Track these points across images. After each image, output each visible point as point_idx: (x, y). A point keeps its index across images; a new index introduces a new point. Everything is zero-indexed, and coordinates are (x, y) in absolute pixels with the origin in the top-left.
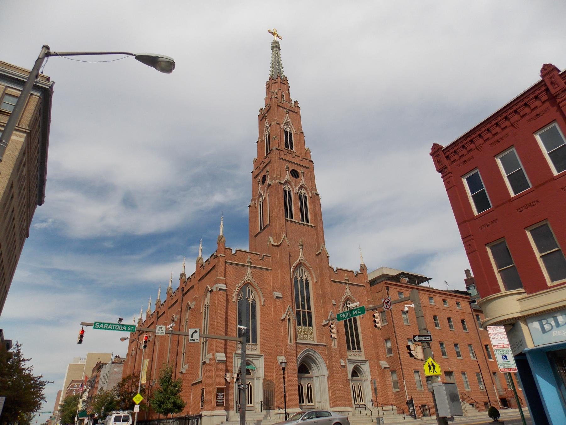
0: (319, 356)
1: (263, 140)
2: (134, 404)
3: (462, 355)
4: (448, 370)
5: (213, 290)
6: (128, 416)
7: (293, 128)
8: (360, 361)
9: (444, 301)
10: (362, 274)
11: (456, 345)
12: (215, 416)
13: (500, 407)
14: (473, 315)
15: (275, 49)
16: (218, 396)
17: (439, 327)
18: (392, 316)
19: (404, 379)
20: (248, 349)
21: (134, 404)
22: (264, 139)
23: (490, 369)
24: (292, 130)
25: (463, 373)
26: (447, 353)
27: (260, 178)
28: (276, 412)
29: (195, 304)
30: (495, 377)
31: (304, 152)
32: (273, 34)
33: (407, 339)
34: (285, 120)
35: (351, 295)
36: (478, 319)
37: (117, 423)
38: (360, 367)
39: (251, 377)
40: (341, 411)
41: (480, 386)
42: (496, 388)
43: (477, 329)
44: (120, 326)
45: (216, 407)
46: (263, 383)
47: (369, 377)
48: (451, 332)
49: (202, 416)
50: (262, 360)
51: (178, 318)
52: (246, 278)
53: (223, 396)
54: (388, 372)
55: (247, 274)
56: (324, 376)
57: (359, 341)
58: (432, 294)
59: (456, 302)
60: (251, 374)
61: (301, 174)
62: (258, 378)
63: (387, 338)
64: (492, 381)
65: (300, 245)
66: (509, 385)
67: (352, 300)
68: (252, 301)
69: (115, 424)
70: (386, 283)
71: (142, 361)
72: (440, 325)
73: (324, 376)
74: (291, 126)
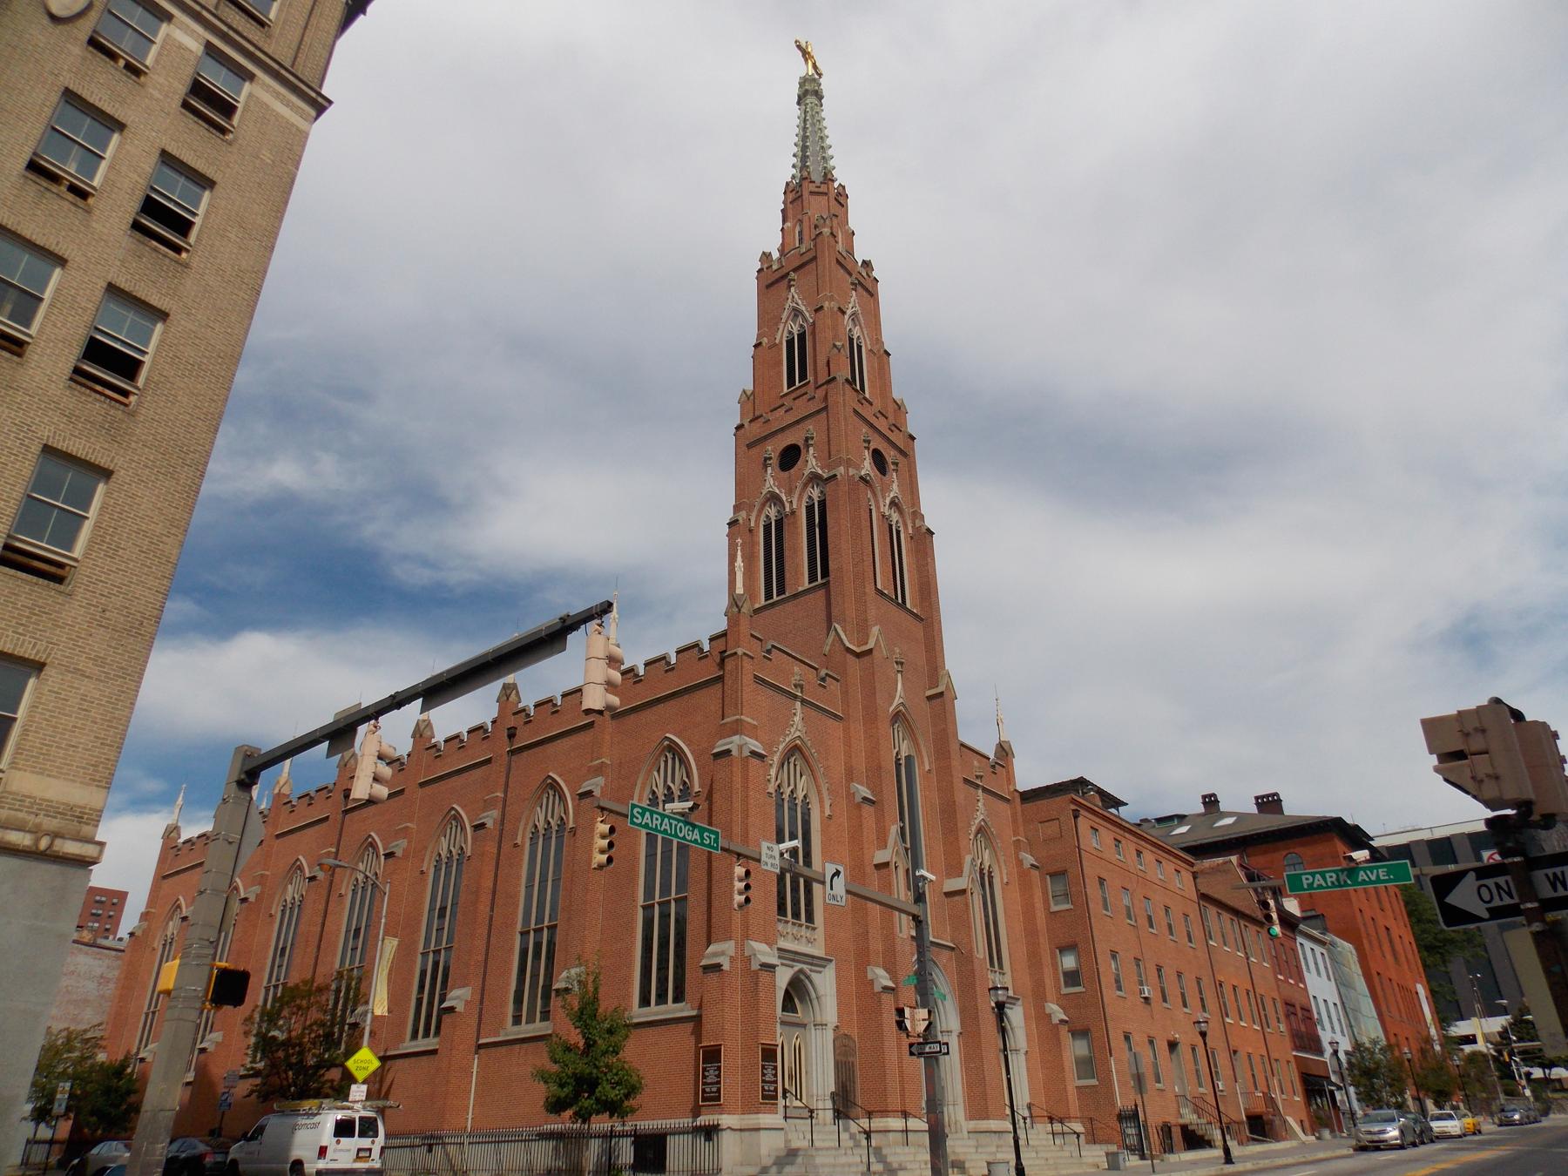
0: (942, 978)
1: (775, 345)
2: (349, 1078)
5: (731, 751)
6: (370, 1118)
7: (865, 332)
8: (810, 960)
10: (1003, 767)
12: (762, 1132)
14: (1199, 906)
15: (811, 99)
16: (706, 1074)
18: (1085, 888)
19: (1111, 1055)
21: (349, 1078)
22: (781, 343)
24: (862, 340)
27: (773, 449)
29: (603, 785)
31: (891, 407)
32: (804, 56)
33: (1111, 951)
34: (850, 306)
37: (343, 1140)
38: (808, 977)
39: (797, 1021)
40: (999, 1132)
44: (687, 828)
45: (761, 1103)
46: (834, 1041)
49: (722, 1130)
51: (495, 819)
53: (717, 1072)
56: (951, 1032)
60: (797, 1013)
61: (892, 467)
63: (1064, 945)
64: (1232, 1072)
65: (897, 663)
69: (338, 1142)
70: (1074, 801)
71: (380, 943)
73: (951, 1032)
74: (860, 326)
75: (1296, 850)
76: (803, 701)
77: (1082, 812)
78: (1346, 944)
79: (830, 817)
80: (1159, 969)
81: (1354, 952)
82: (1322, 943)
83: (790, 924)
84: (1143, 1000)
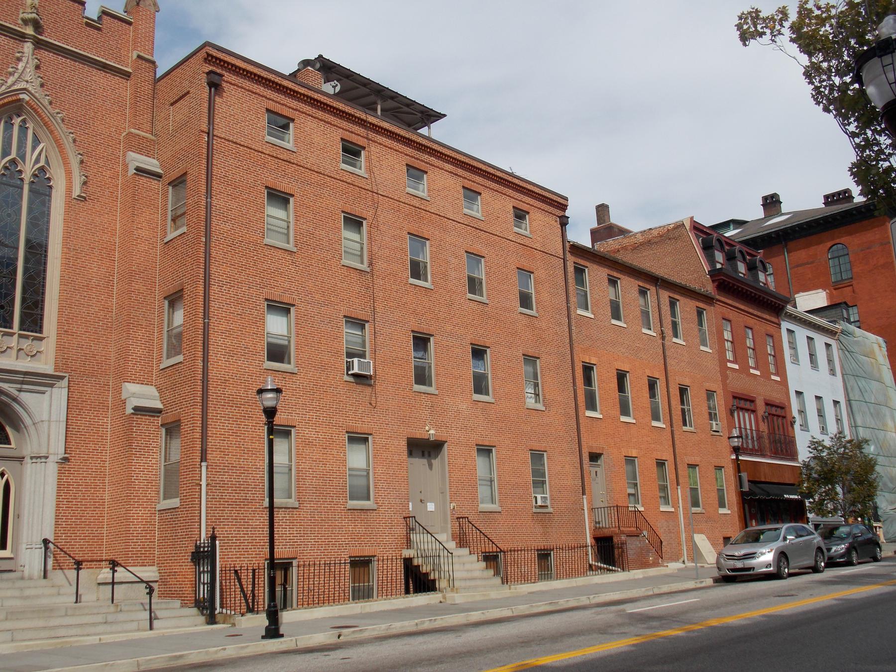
3: (494, 390)
4: (426, 437)
8: (19, 378)
9: (520, 215)
10: (130, 23)
11: (478, 353)
13: (590, 566)
17: (426, 280)
19: (203, 458)
20: (32, 356)
23: (583, 443)
25: (485, 451)
26: (437, 375)
28: (106, 575)
30: (593, 470)
35: (39, 93)
36: (580, 281)
38: (15, 400)
41: (536, 498)
42: (590, 502)
43: (568, 308)
47: (58, 448)
48: (472, 304)
50: (59, 395)
52: (11, 80)
54: (153, 428)
55: (21, 66)
57: (43, 293)
58: (426, 157)
59: (342, 139)
62: (37, 458)
66: (633, 495)
67: (40, 116)
68: (35, 175)
72: (432, 275)
75: (842, 240)
76: (39, 44)
77: (228, 76)
78: (872, 337)
79: (82, 199)
80: (621, 377)
81: (884, 345)
82: (831, 333)
83: (16, 336)
84: (351, 379)
